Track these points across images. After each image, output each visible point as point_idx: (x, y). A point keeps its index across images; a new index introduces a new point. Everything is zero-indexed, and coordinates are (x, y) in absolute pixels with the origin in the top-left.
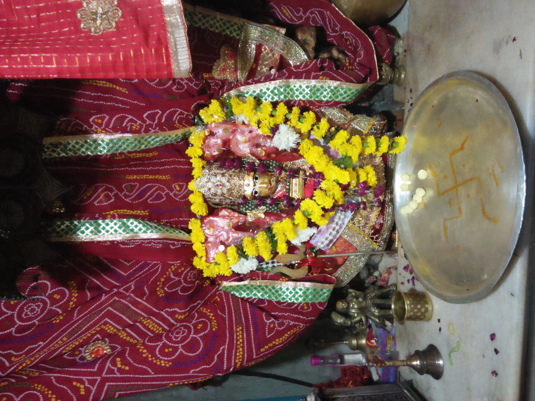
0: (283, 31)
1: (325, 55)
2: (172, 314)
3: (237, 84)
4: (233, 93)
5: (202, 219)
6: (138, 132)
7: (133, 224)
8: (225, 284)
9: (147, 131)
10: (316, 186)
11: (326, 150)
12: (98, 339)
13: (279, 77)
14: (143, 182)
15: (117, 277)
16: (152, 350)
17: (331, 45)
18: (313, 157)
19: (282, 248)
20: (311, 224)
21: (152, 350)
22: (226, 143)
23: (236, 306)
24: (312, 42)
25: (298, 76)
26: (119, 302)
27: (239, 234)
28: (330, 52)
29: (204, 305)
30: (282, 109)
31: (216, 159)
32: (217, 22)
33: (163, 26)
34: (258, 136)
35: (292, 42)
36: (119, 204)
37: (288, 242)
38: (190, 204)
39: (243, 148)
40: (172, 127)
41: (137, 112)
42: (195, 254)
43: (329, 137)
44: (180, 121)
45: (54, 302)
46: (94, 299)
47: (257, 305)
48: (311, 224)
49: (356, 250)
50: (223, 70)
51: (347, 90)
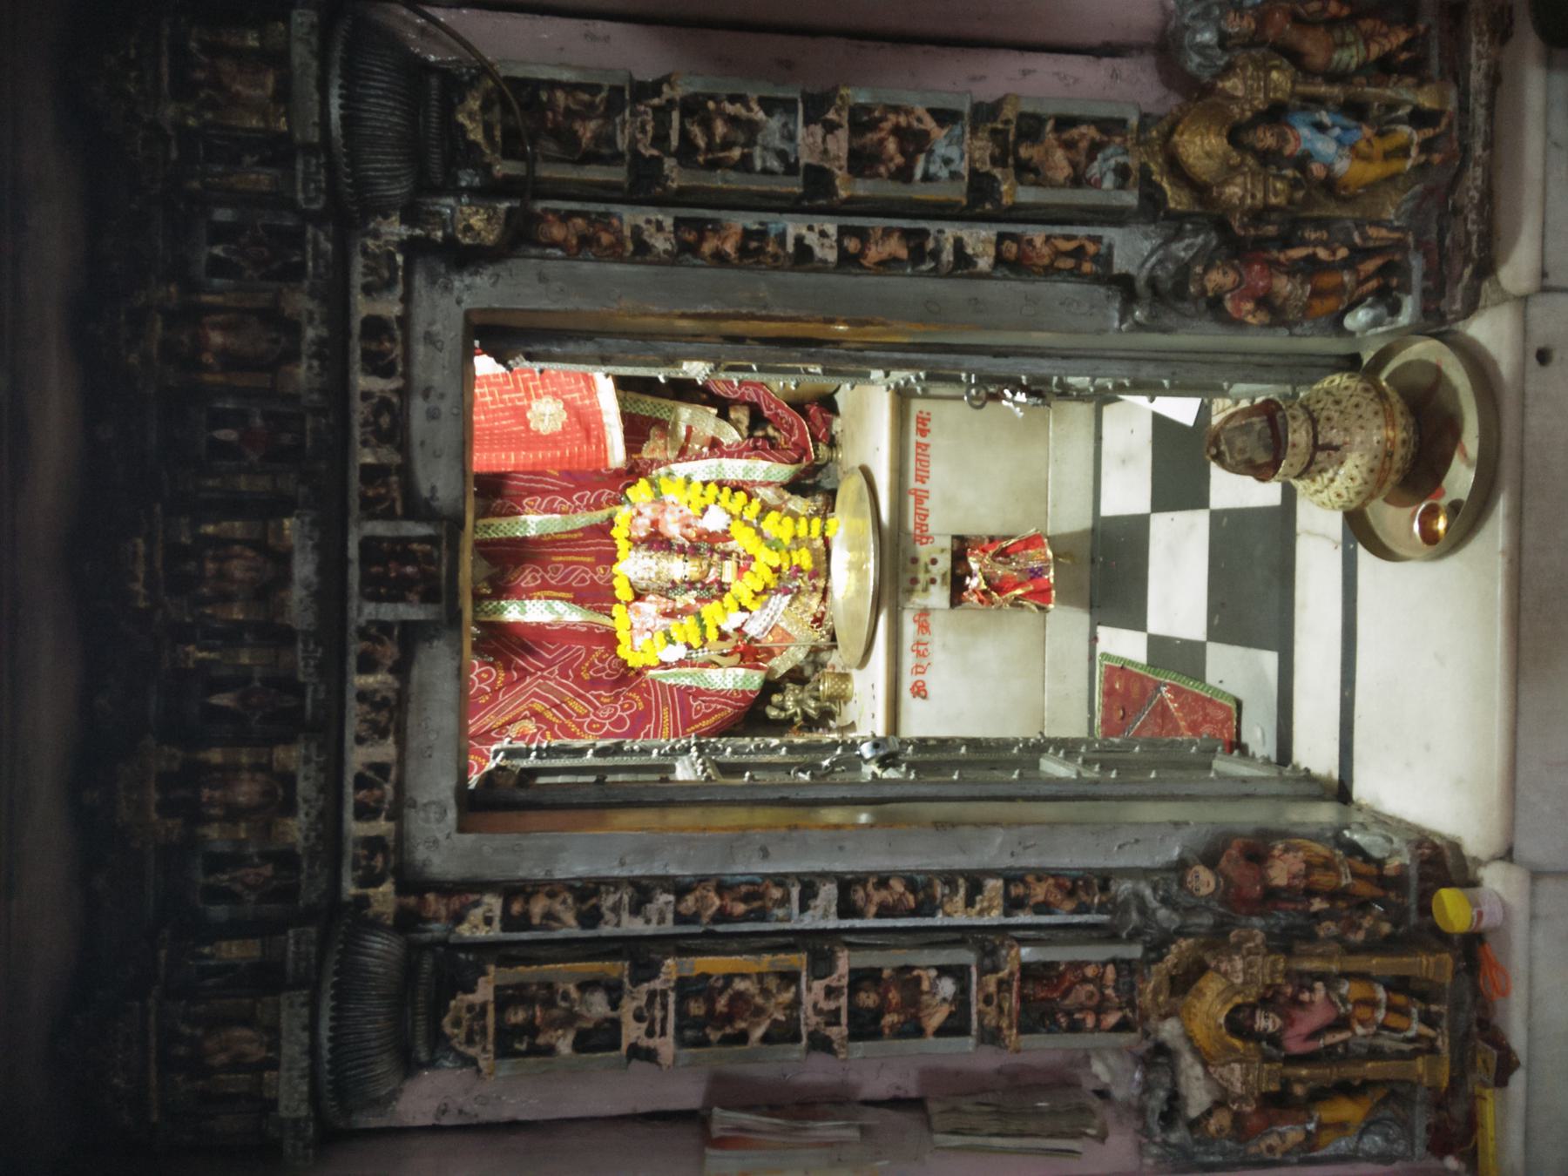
0: (714, 411)
1: (759, 433)
2: (598, 697)
3: (667, 462)
4: (662, 470)
5: (628, 604)
6: (566, 513)
7: (559, 606)
8: (651, 672)
9: (575, 512)
10: (747, 568)
11: (759, 532)
12: (525, 717)
13: (712, 456)
14: (567, 564)
15: (541, 659)
16: (580, 726)
17: (767, 421)
18: (744, 540)
19: (712, 635)
20: (743, 609)
21: (580, 726)
22: (654, 523)
23: (663, 692)
24: (745, 421)
25: (730, 455)
26: (542, 684)
27: (667, 621)
28: (764, 429)
29: (631, 690)
30: (712, 488)
31: (643, 541)
32: (647, 405)
33: (601, 426)
34: (688, 517)
35: (723, 423)
36: (545, 586)
37: (718, 628)
38: (613, 588)
39: (672, 529)
40: (599, 507)
41: (567, 493)
42: (618, 642)
43: (760, 518)
44: (608, 502)
45: (482, 681)
46: (521, 679)
47: (685, 692)
48: (743, 609)
49: (794, 639)
50: (652, 449)
51: (783, 471)
